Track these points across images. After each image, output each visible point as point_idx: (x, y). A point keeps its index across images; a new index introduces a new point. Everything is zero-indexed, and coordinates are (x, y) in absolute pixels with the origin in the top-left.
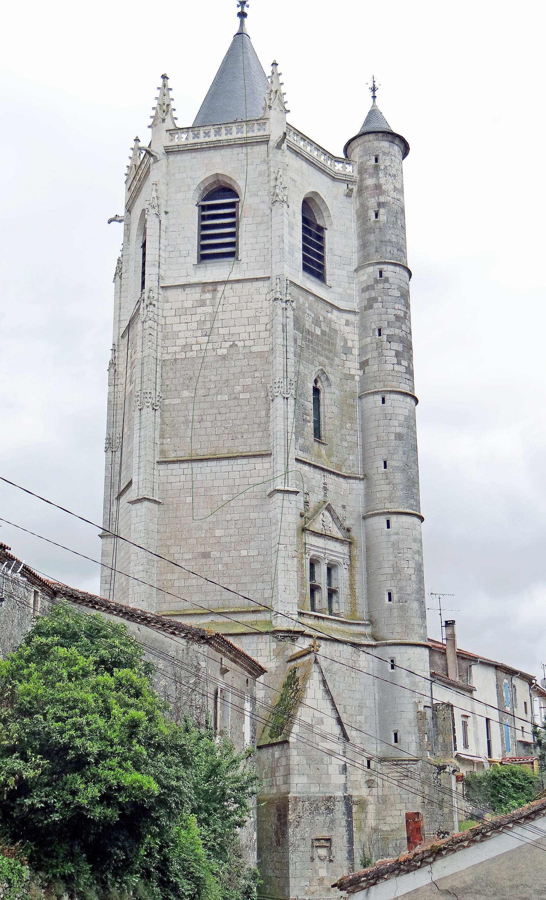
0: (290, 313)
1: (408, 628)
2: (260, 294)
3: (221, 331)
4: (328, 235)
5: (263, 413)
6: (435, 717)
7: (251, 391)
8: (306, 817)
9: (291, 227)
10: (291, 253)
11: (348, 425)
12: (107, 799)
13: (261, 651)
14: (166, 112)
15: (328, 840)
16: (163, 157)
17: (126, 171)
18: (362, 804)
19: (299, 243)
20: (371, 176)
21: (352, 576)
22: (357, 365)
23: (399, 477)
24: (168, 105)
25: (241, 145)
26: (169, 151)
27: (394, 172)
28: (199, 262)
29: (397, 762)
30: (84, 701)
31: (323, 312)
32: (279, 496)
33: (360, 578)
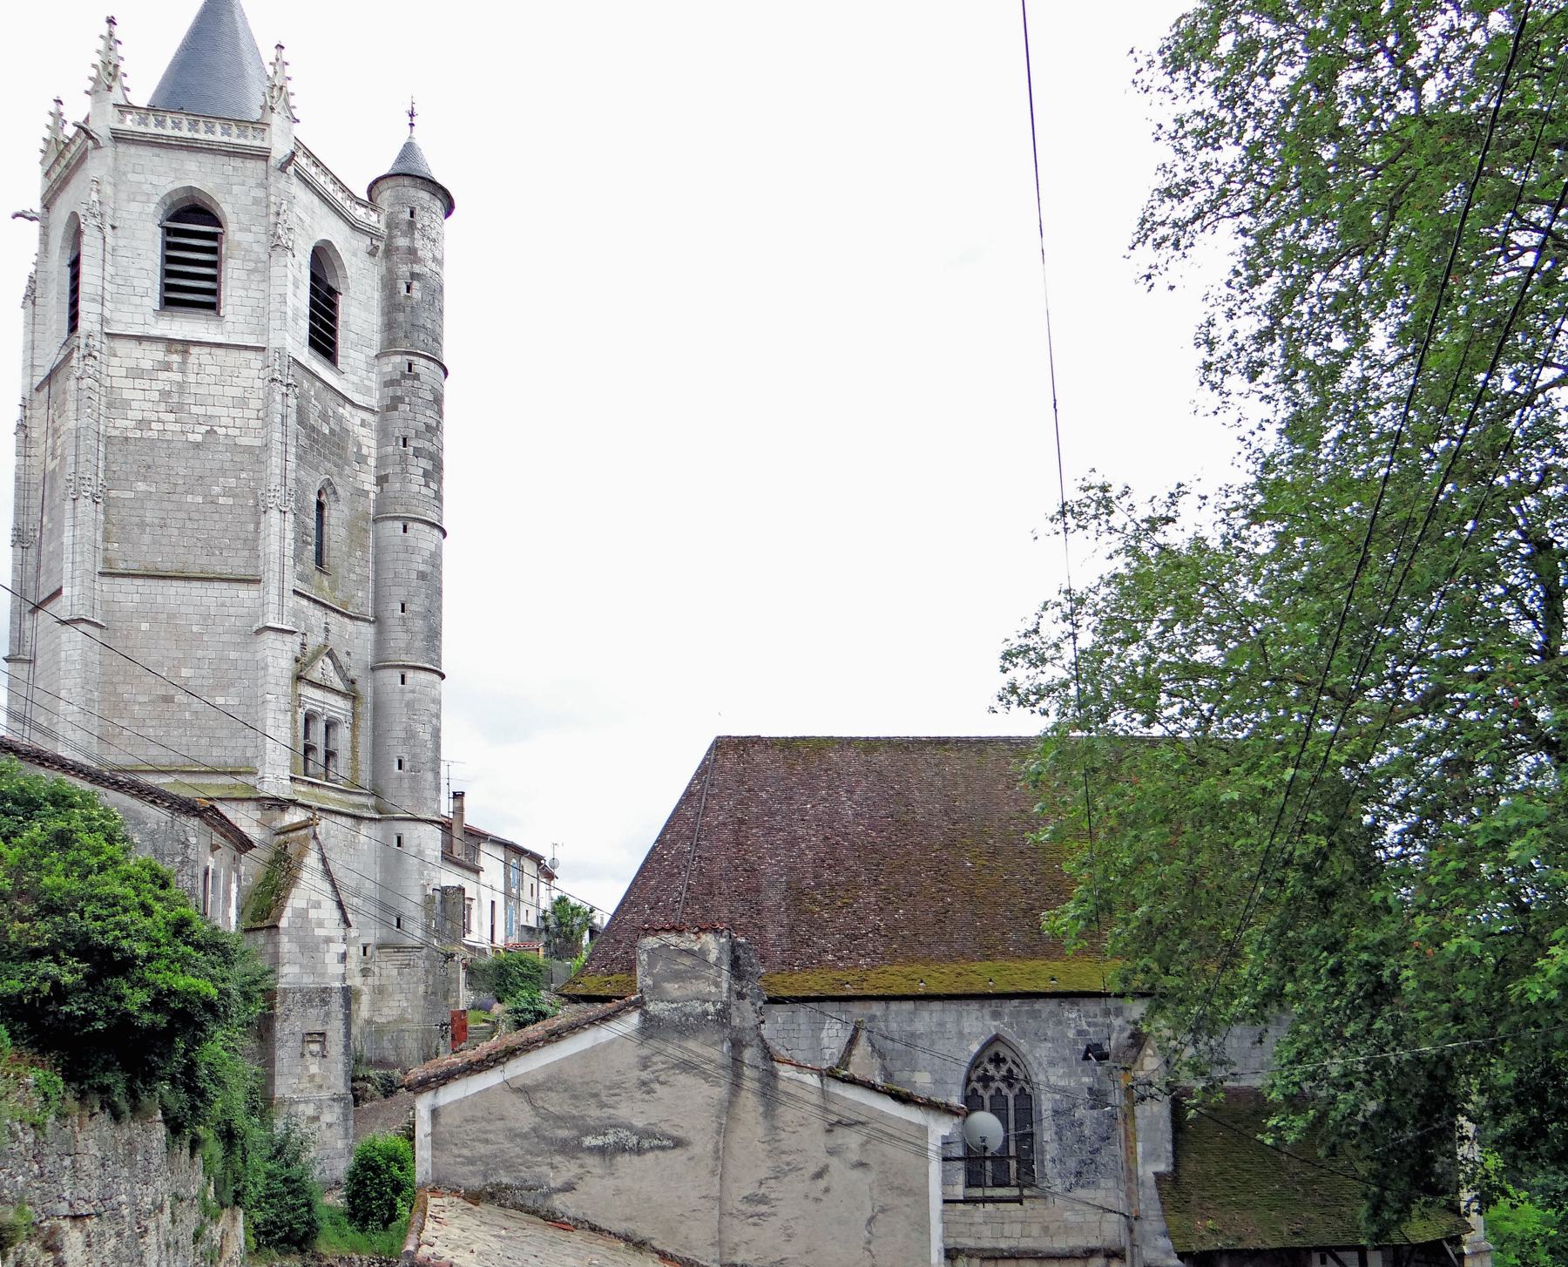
0: (292, 401)
1: (420, 802)
2: (251, 371)
3: (194, 409)
4: (342, 301)
5: (251, 527)
6: (443, 901)
7: (234, 496)
8: (297, 1010)
9: (296, 285)
10: (295, 320)
11: (358, 554)
12: (157, 1004)
13: (246, 820)
14: (113, 76)
15: (322, 1034)
16: (109, 143)
17: (42, 145)
18: (358, 993)
19: (305, 309)
20: (404, 235)
21: (354, 736)
22: (373, 479)
23: (419, 624)
24: (116, 66)
25: (229, 154)
26: (118, 137)
27: (434, 235)
28: (162, 308)
29: (399, 948)
30: (125, 898)
31: (332, 404)
32: (272, 635)
33: (365, 740)
